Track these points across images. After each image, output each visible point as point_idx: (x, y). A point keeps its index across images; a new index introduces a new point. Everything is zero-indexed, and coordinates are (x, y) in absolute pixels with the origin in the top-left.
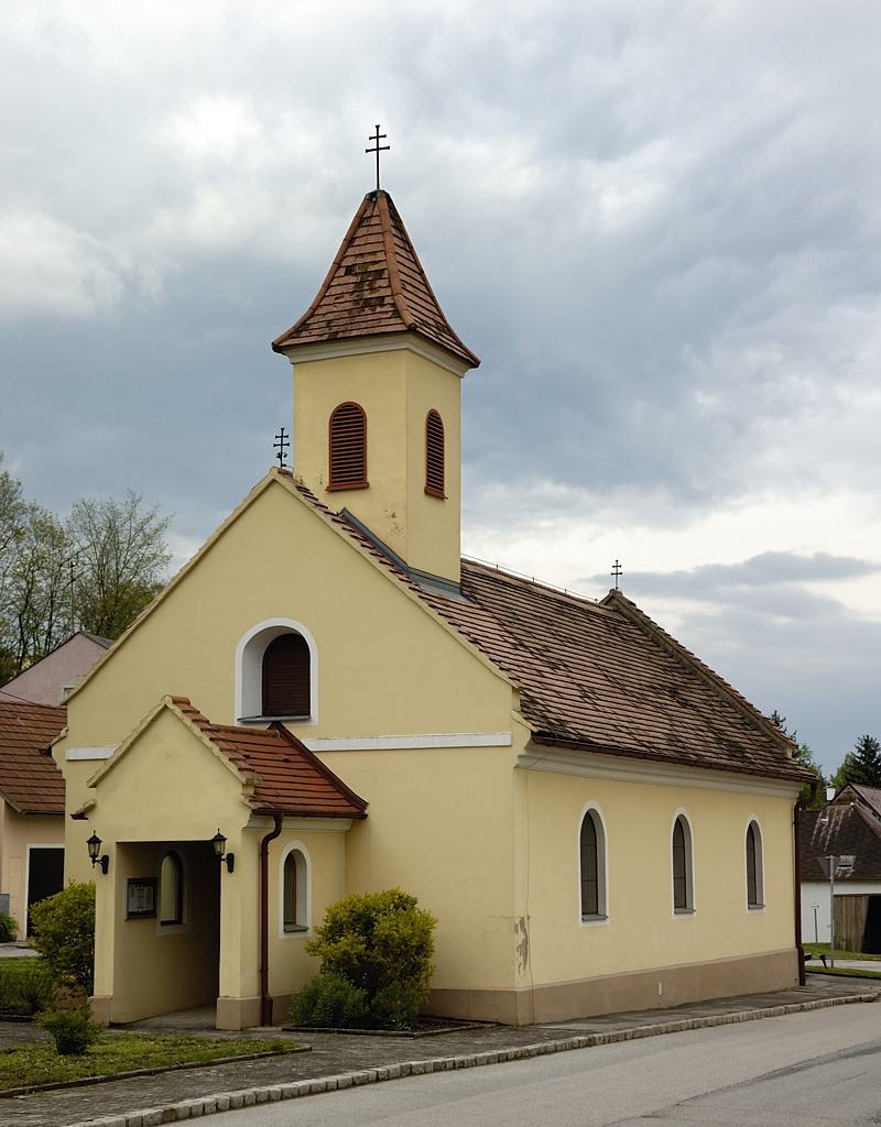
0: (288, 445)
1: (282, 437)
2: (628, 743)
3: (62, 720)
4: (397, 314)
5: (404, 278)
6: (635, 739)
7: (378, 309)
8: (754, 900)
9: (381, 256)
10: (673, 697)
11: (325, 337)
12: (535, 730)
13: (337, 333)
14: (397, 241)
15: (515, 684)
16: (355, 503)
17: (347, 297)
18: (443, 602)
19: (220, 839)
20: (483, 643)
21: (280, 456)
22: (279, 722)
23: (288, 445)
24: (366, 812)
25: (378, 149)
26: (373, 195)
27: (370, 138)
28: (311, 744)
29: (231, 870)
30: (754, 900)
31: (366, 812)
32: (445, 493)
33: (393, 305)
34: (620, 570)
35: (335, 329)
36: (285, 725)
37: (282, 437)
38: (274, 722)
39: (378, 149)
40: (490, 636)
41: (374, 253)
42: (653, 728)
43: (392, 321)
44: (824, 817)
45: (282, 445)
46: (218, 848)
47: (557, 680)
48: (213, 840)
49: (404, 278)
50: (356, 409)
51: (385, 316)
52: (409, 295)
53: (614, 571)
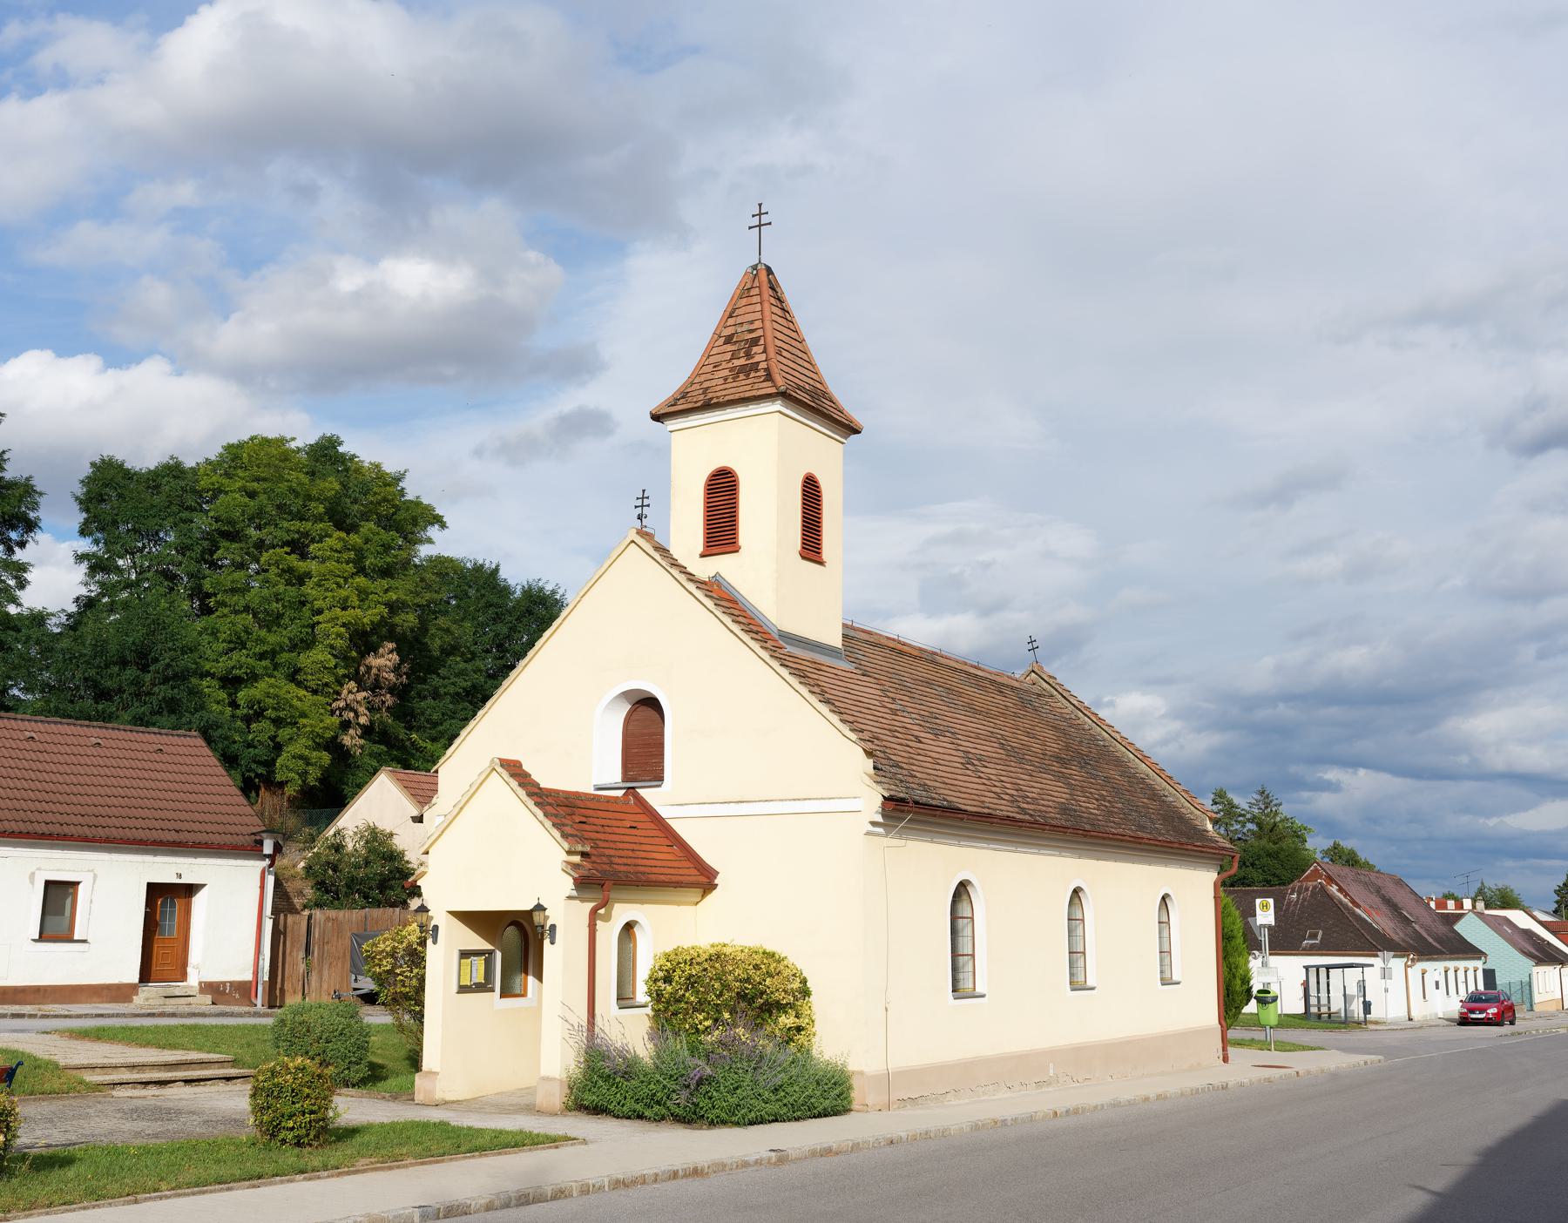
0: (648, 506)
1: (643, 498)
2: (1004, 809)
3: (433, 787)
4: (769, 377)
5: (779, 343)
6: (1019, 807)
7: (752, 375)
8: (1372, 965)
9: (758, 324)
10: (1082, 767)
11: (699, 404)
12: (886, 795)
13: (712, 399)
14: (775, 310)
15: (869, 746)
16: (722, 565)
17: (724, 365)
18: (816, 666)
19: (540, 908)
20: (837, 703)
21: (640, 517)
22: (633, 788)
23: (648, 506)
24: (716, 882)
25: (760, 226)
26: (755, 267)
27: (753, 216)
28: (664, 812)
29: (552, 943)
30: (1372, 965)
31: (716, 882)
32: (824, 557)
33: (765, 370)
34: (1035, 645)
35: (710, 396)
36: (638, 790)
37: (643, 498)
38: (629, 788)
39: (760, 226)
40: (865, 700)
41: (752, 322)
42: (1049, 793)
43: (765, 384)
44: (1292, 893)
45: (642, 506)
46: (538, 918)
47: (937, 747)
48: (532, 911)
49: (779, 343)
50: (730, 473)
51: (758, 381)
52: (785, 361)
53: (1030, 646)
